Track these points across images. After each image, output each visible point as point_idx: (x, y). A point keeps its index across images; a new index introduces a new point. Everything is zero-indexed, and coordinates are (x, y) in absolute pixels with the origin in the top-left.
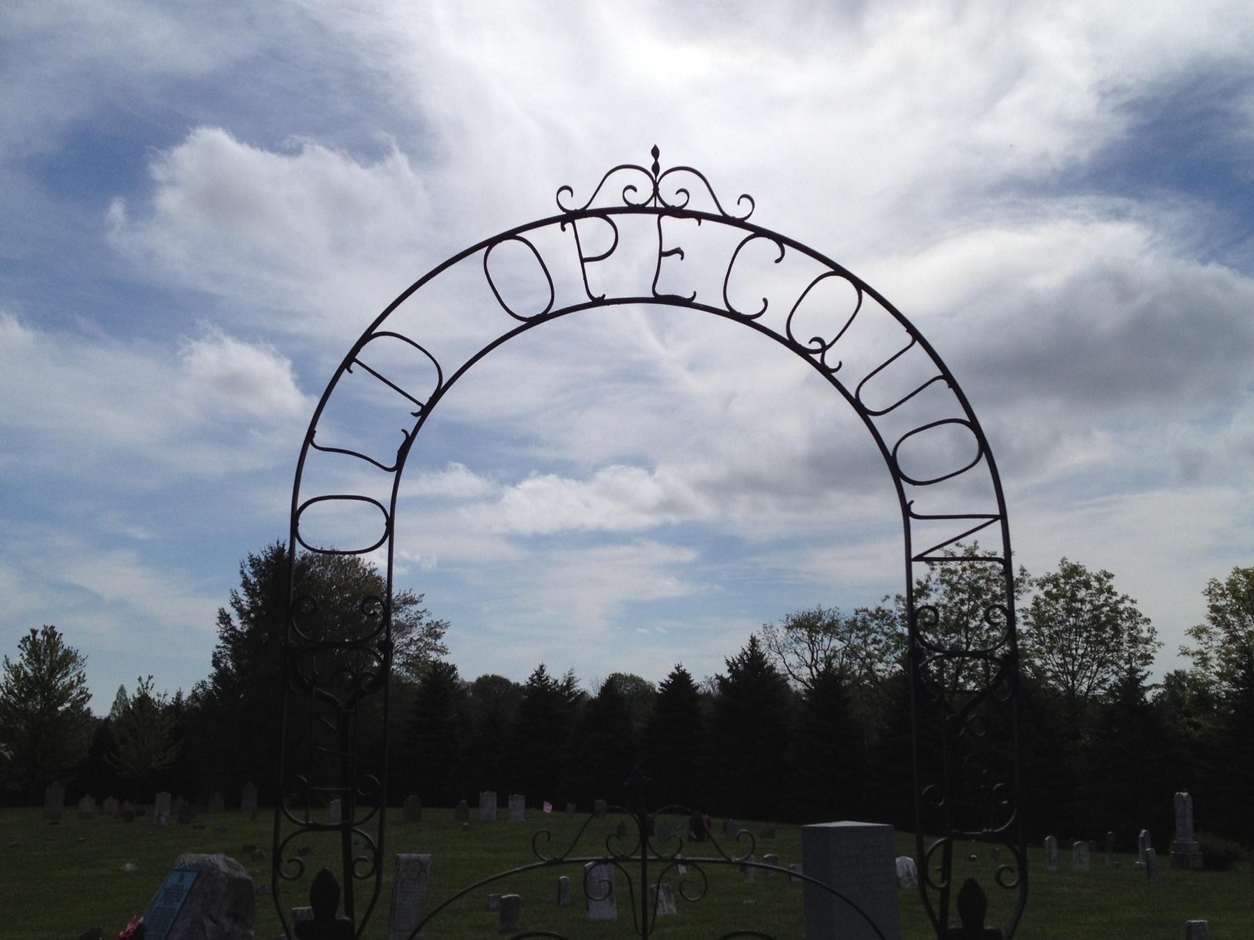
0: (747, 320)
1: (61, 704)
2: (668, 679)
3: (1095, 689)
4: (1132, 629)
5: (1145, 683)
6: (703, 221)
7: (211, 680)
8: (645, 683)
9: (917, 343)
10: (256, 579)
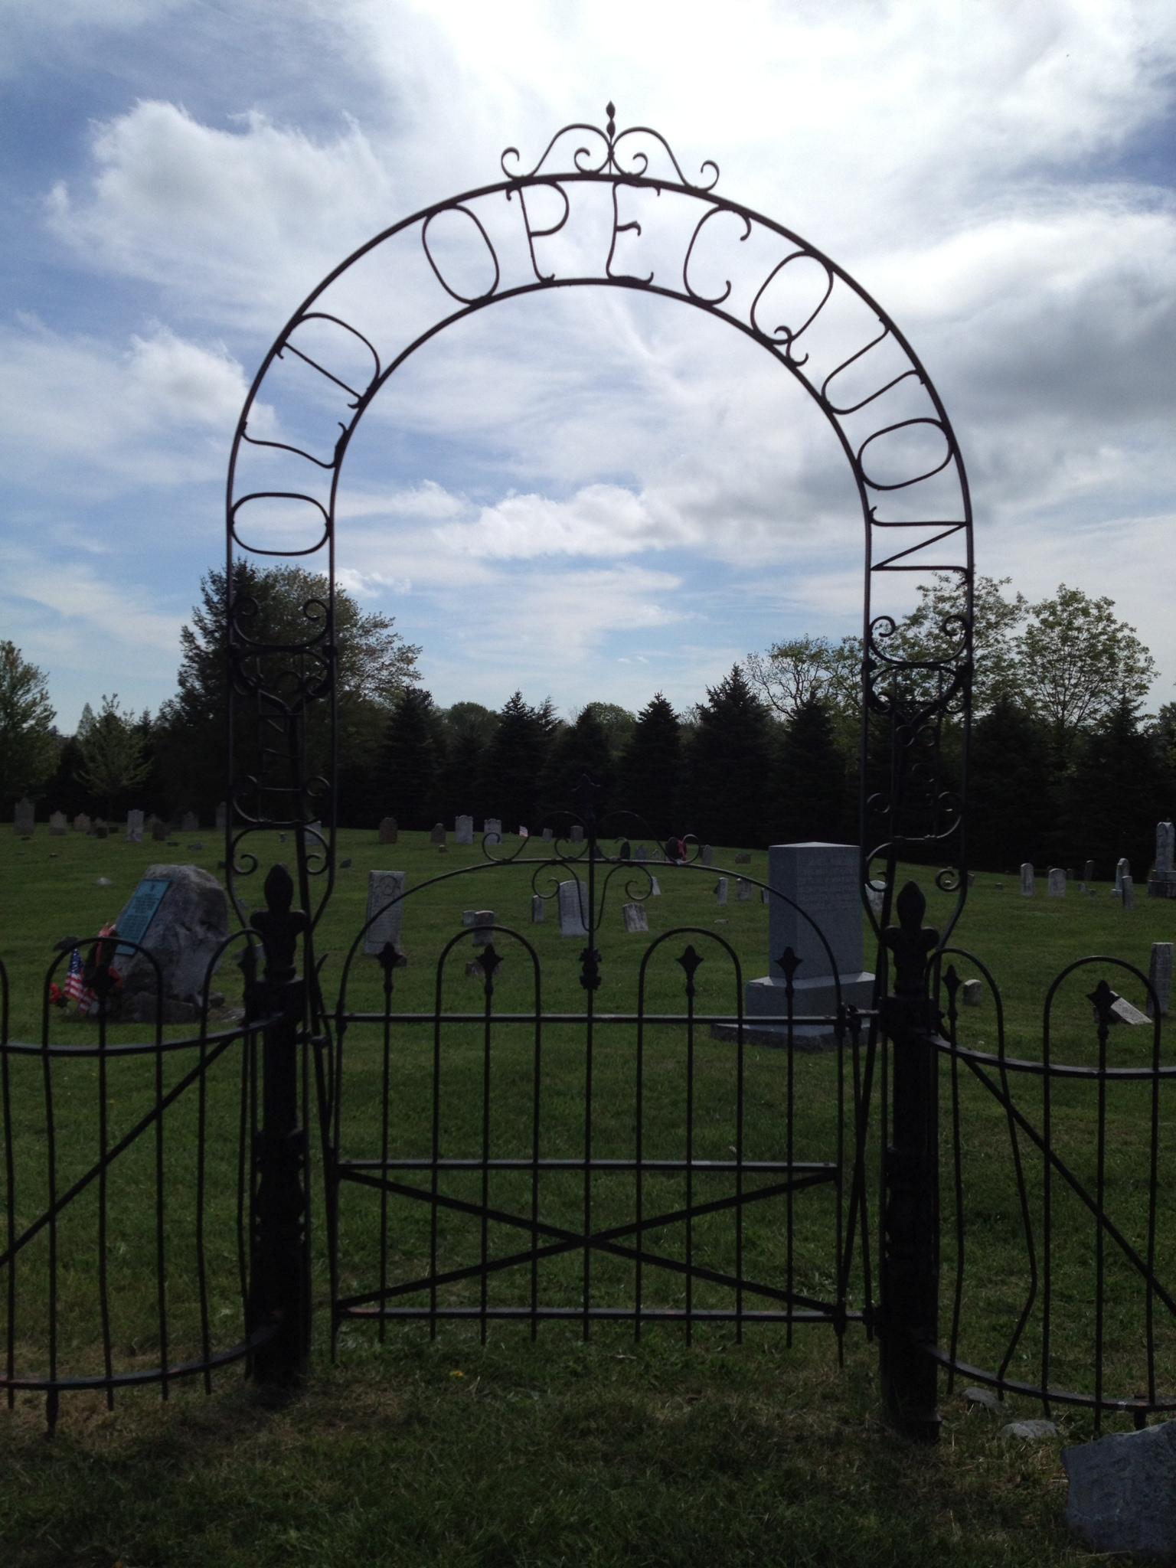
1: (25, 721)
3: (1085, 719)
5: (1137, 714)
7: (178, 700)
9: (890, 333)
10: (218, 597)
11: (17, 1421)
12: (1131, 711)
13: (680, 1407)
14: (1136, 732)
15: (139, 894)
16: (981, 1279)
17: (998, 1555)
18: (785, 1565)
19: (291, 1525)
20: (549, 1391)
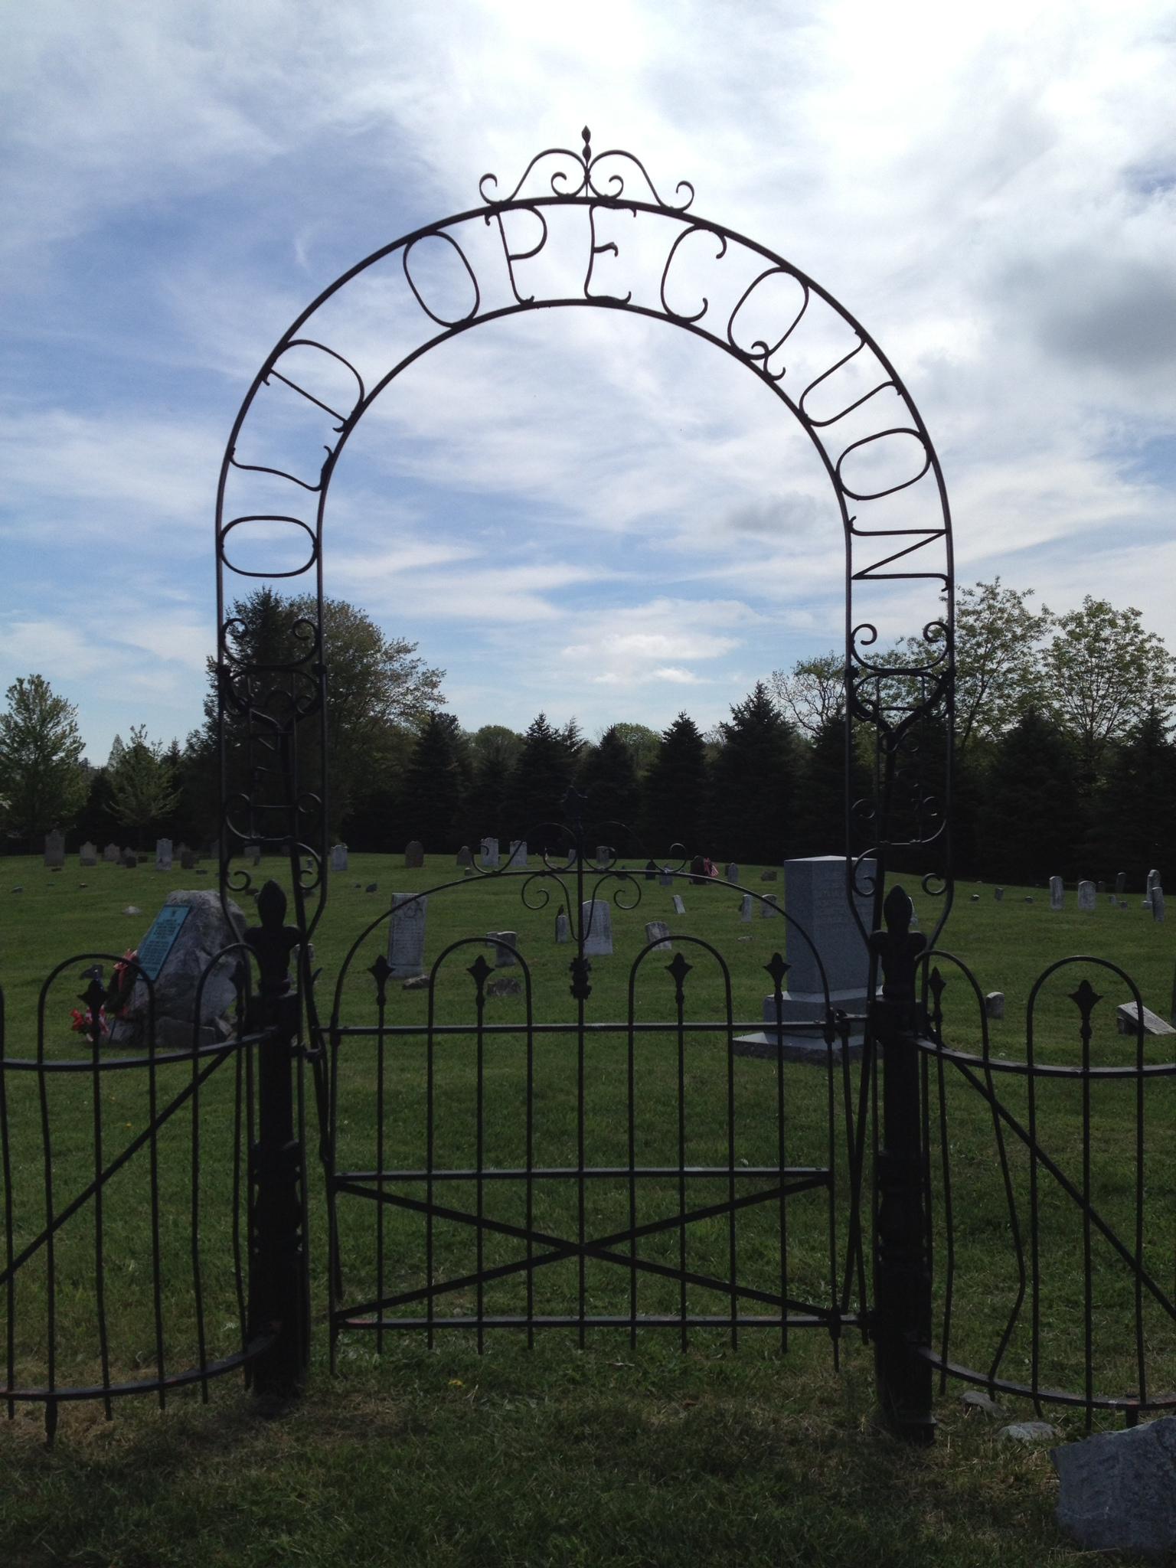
0: (685, 323)
1: (55, 754)
2: (672, 727)
4: (1157, 669)
5: (1167, 724)
6: (638, 212)
7: (205, 729)
8: (651, 732)
9: (866, 345)
11: (17, 1432)
12: (1161, 721)
13: (677, 1413)
14: (1166, 742)
15: (161, 920)
16: (986, 1285)
17: (987, 1553)
18: (771, 1564)
19: (282, 1530)
20: (546, 1399)
